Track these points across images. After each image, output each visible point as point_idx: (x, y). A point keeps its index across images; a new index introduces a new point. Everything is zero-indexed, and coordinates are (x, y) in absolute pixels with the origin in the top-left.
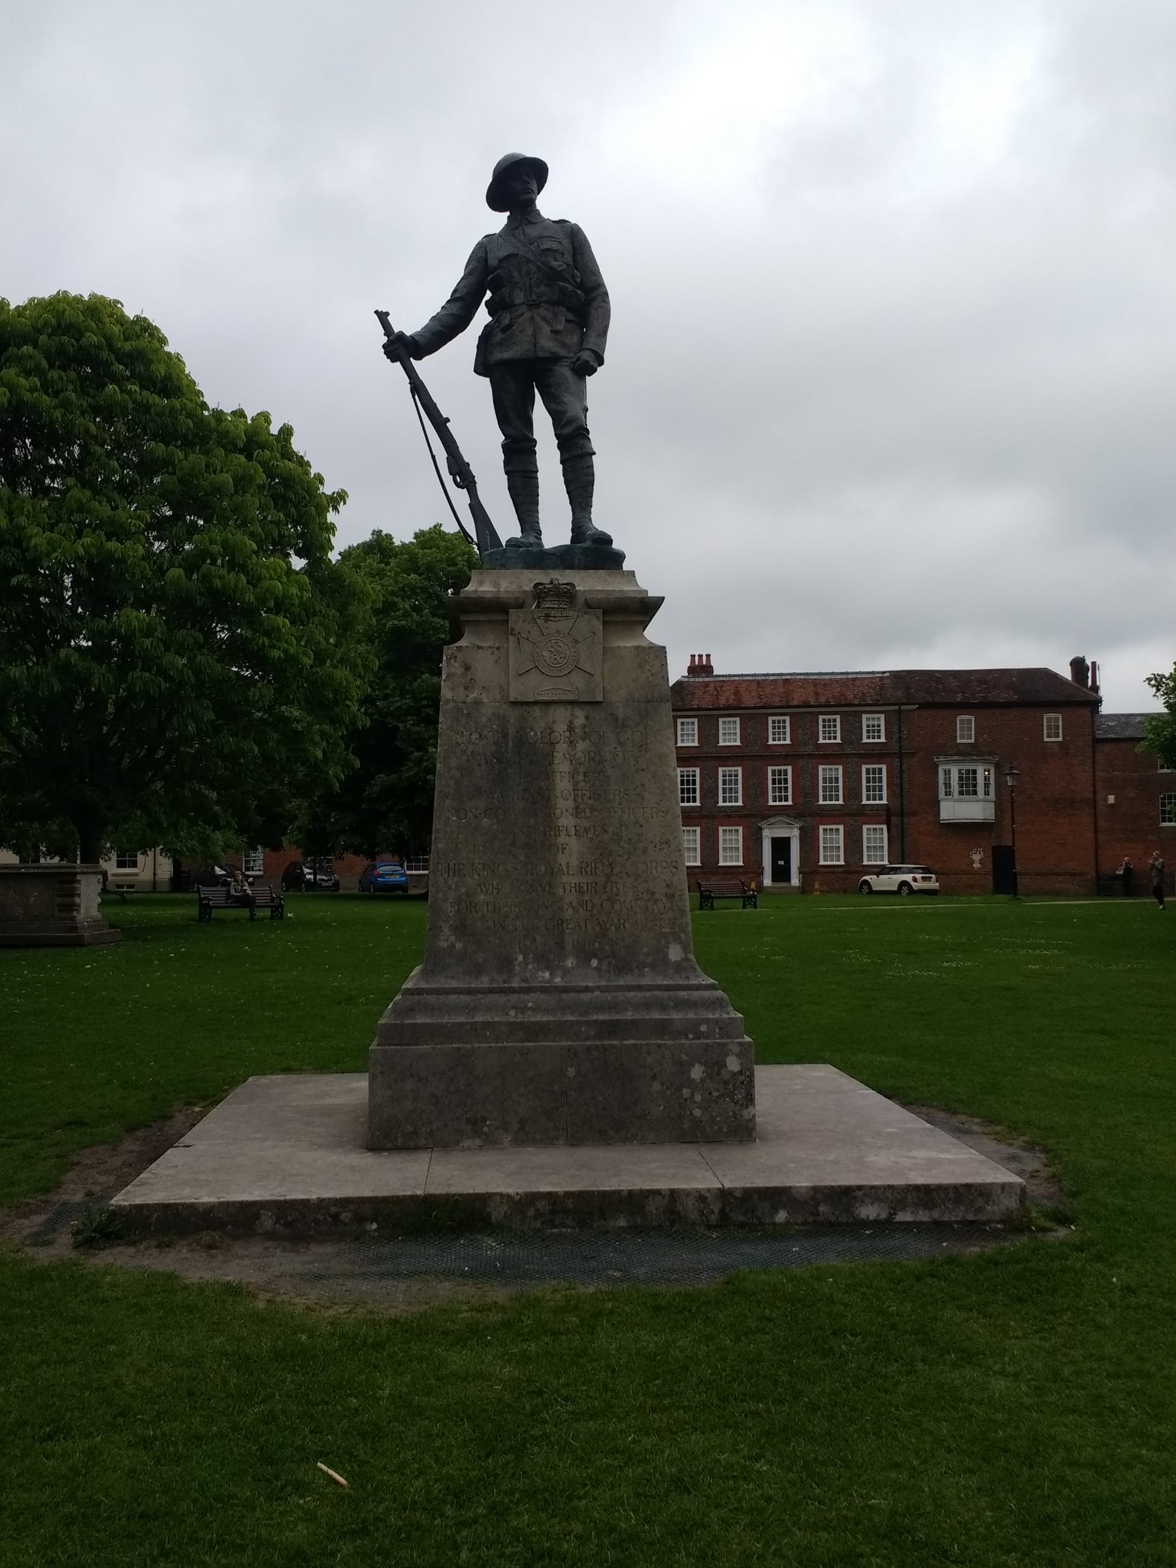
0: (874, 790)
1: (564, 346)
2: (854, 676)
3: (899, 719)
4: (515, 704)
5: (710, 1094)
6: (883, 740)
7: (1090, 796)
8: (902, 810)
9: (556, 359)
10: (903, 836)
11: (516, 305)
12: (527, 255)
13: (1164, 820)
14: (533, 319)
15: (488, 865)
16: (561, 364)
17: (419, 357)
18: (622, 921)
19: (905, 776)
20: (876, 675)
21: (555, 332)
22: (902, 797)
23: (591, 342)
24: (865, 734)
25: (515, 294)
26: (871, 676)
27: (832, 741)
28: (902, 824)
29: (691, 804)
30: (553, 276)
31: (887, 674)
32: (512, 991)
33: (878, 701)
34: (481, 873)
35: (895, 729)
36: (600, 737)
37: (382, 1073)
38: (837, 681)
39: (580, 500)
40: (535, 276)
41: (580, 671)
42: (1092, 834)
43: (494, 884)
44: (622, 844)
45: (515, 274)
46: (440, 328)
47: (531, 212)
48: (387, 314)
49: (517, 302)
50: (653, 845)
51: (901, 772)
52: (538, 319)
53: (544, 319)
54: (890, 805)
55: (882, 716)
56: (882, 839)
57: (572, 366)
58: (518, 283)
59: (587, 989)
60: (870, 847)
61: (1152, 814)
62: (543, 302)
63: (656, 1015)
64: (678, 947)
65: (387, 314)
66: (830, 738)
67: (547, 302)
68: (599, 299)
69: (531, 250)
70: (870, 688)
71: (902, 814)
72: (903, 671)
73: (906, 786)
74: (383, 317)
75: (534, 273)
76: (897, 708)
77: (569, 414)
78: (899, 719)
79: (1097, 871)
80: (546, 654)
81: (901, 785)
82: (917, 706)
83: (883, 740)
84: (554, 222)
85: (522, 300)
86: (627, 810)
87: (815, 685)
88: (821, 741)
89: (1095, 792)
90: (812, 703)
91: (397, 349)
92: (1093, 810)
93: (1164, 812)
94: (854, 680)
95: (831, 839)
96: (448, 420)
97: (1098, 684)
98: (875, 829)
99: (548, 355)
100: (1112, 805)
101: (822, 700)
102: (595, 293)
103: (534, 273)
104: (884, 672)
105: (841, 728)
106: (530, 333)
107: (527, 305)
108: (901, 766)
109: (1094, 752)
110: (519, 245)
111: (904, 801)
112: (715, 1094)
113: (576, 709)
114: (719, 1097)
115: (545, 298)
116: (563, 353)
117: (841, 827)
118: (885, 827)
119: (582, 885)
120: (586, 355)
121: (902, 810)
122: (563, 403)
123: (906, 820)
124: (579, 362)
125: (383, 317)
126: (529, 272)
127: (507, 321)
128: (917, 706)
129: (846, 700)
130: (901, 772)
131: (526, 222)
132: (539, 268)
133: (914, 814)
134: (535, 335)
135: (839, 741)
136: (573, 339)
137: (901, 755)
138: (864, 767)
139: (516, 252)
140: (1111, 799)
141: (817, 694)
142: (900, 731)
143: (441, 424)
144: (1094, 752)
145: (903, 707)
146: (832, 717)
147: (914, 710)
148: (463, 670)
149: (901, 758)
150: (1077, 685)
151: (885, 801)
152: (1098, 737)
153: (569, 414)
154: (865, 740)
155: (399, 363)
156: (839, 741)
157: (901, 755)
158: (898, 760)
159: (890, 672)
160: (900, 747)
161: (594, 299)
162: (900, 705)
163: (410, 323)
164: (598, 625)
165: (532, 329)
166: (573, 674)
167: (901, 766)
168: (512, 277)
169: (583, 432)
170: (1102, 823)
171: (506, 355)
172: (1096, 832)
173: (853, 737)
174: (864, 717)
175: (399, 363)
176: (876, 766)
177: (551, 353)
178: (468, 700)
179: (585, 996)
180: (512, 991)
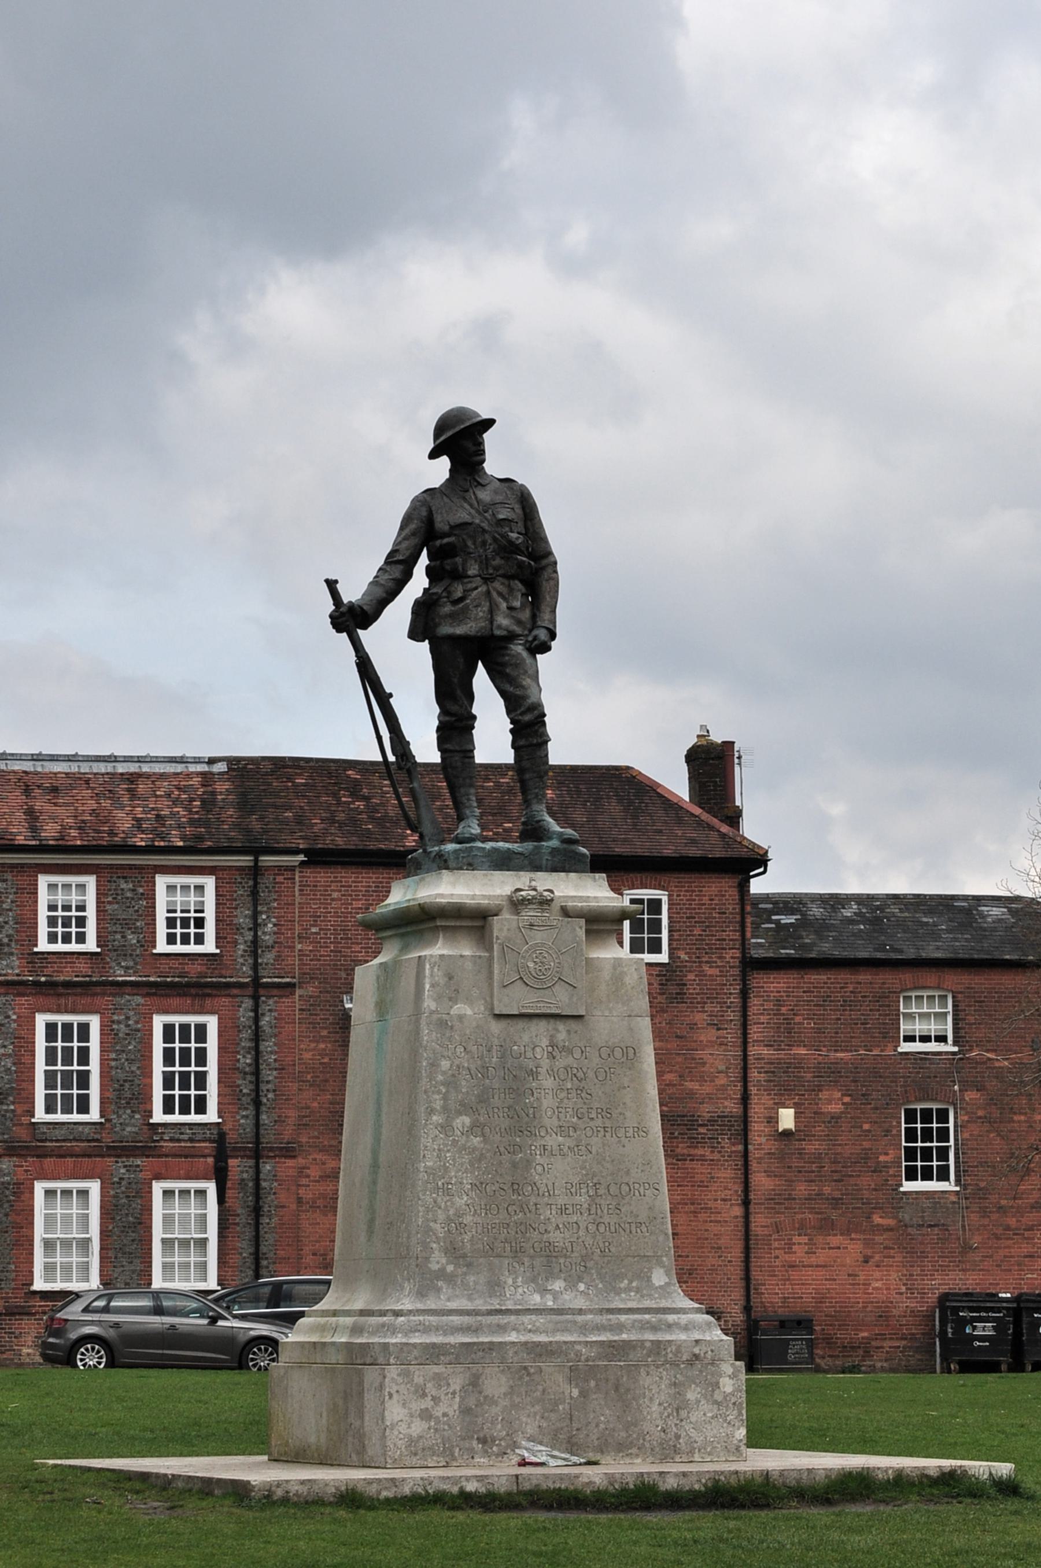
0: (185, 1085)
1: (519, 622)
2: (133, 768)
3: (254, 893)
4: (499, 1017)
5: (704, 1414)
6: (210, 946)
7: (732, 1106)
8: (257, 1140)
9: (511, 637)
10: (257, 1211)
11: (469, 577)
12: (483, 525)
13: (911, 1175)
14: (488, 593)
15: (475, 1185)
16: (516, 642)
17: (365, 627)
18: (607, 1244)
19: (267, 1045)
20: (193, 768)
21: (511, 608)
22: (257, 1103)
23: (544, 619)
24: (161, 931)
25: (469, 564)
26: (179, 768)
27: (74, 947)
28: (257, 1180)
29: (193, 1118)
30: (508, 549)
31: (221, 767)
32: (508, 1312)
33: (200, 838)
34: (470, 1193)
35: (243, 918)
36: (582, 1052)
37: (397, 1392)
38: (85, 780)
39: (537, 791)
40: (492, 547)
41: (563, 983)
42: (738, 1211)
43: (483, 1203)
44: (605, 1164)
45: (470, 543)
46: (384, 595)
47: (480, 471)
48: (336, 582)
49: (470, 573)
50: (636, 1165)
51: (257, 1037)
52: (494, 594)
53: (500, 594)
54: (226, 1128)
55: (209, 883)
56: (202, 1220)
57: (527, 645)
58: (472, 553)
59: (581, 1312)
60: (172, 1241)
61: (882, 1158)
62: (499, 576)
63: (651, 1337)
64: (662, 1271)
65: (336, 582)
66: (67, 939)
67: (504, 576)
68: (550, 570)
69: (486, 519)
70: (176, 802)
71: (257, 1154)
72: (264, 758)
73: (268, 1075)
74: (331, 585)
75: (490, 544)
76: (246, 860)
77: (530, 701)
78: (254, 893)
79: (747, 1309)
80: (531, 965)
81: (257, 1073)
82: (301, 858)
83: (210, 946)
84: (500, 480)
85: (476, 572)
86: (609, 1130)
87: (27, 791)
88: (43, 945)
89: (745, 1099)
90: (20, 840)
91: (346, 621)
92: (740, 1147)
93: (911, 1154)
94: (132, 778)
95: (67, 1219)
96: (391, 695)
97: (738, 803)
98: (185, 1193)
99: (504, 633)
100: (787, 1133)
101: (49, 832)
102: (544, 562)
103: (490, 544)
104: (212, 761)
105: (98, 911)
106: (485, 609)
107: (483, 578)
108: (256, 1019)
109: (744, 994)
110: (473, 512)
111: (264, 1117)
112: (710, 1415)
113: (558, 1023)
114: (712, 1418)
115: (501, 572)
116: (518, 630)
117: (94, 1187)
118: (211, 1188)
119: (567, 1206)
120: (543, 635)
121: (257, 1140)
122: (523, 687)
123: (267, 1167)
124: (536, 642)
125: (331, 585)
126: (484, 543)
127: (459, 594)
128: (301, 858)
129: (112, 833)
130: (257, 1037)
131: (475, 484)
132: (495, 539)
133: (288, 1152)
134: (491, 611)
135: (91, 945)
136: (526, 615)
137: (256, 988)
138: (159, 1022)
139: (470, 521)
140: (787, 1119)
141: (32, 815)
142: (256, 926)
143: (384, 699)
144: (744, 994)
145: (267, 860)
146: (73, 879)
147: (292, 869)
148: (446, 979)
149: (256, 998)
150: (697, 811)
151: (212, 1116)
152: (756, 953)
153: (530, 701)
154: (162, 946)
155: (345, 634)
156: (91, 945)
157: (256, 988)
158: (248, 1003)
159: (231, 761)
160: (255, 966)
161: (543, 568)
162: (257, 852)
163: (353, 592)
164: (581, 933)
165: (488, 604)
166: (557, 986)
167: (256, 1019)
168: (466, 546)
169: (540, 719)
170: (761, 1181)
171: (459, 630)
172: (746, 1203)
173: (132, 938)
174: (162, 882)
175: (345, 634)
176: (192, 1019)
177: (509, 632)
178: (452, 1013)
179: (579, 1318)
180: (508, 1312)
